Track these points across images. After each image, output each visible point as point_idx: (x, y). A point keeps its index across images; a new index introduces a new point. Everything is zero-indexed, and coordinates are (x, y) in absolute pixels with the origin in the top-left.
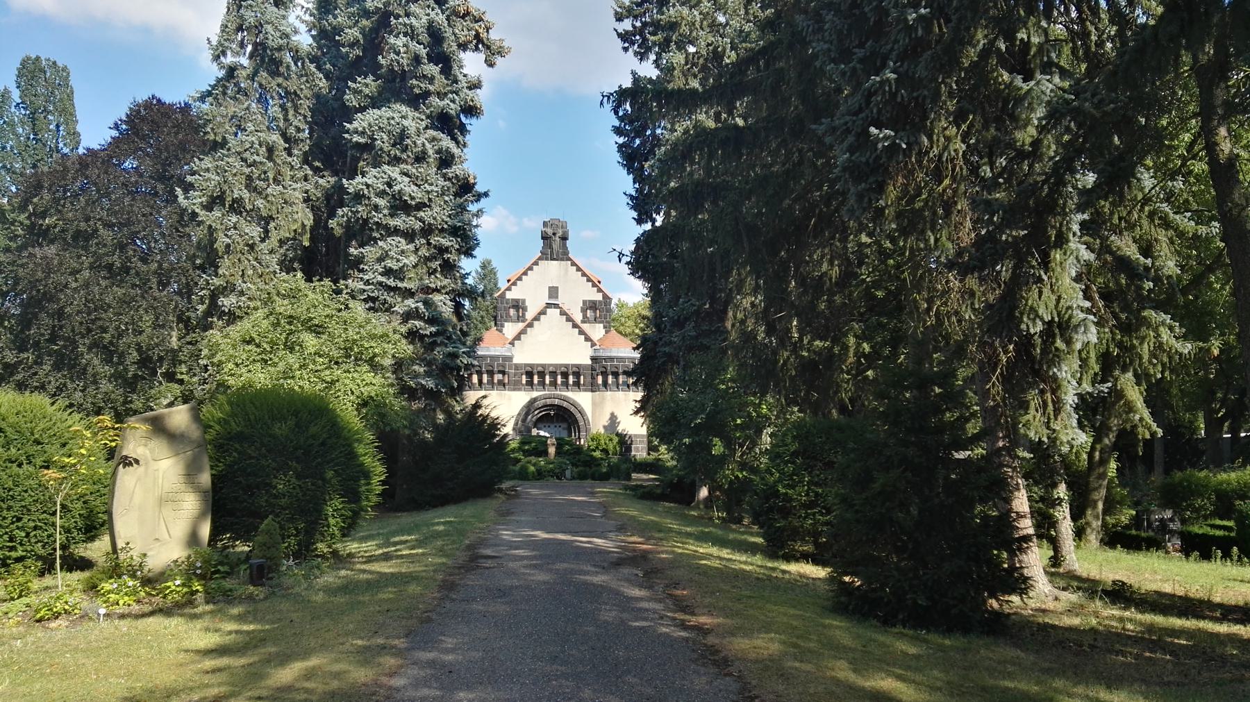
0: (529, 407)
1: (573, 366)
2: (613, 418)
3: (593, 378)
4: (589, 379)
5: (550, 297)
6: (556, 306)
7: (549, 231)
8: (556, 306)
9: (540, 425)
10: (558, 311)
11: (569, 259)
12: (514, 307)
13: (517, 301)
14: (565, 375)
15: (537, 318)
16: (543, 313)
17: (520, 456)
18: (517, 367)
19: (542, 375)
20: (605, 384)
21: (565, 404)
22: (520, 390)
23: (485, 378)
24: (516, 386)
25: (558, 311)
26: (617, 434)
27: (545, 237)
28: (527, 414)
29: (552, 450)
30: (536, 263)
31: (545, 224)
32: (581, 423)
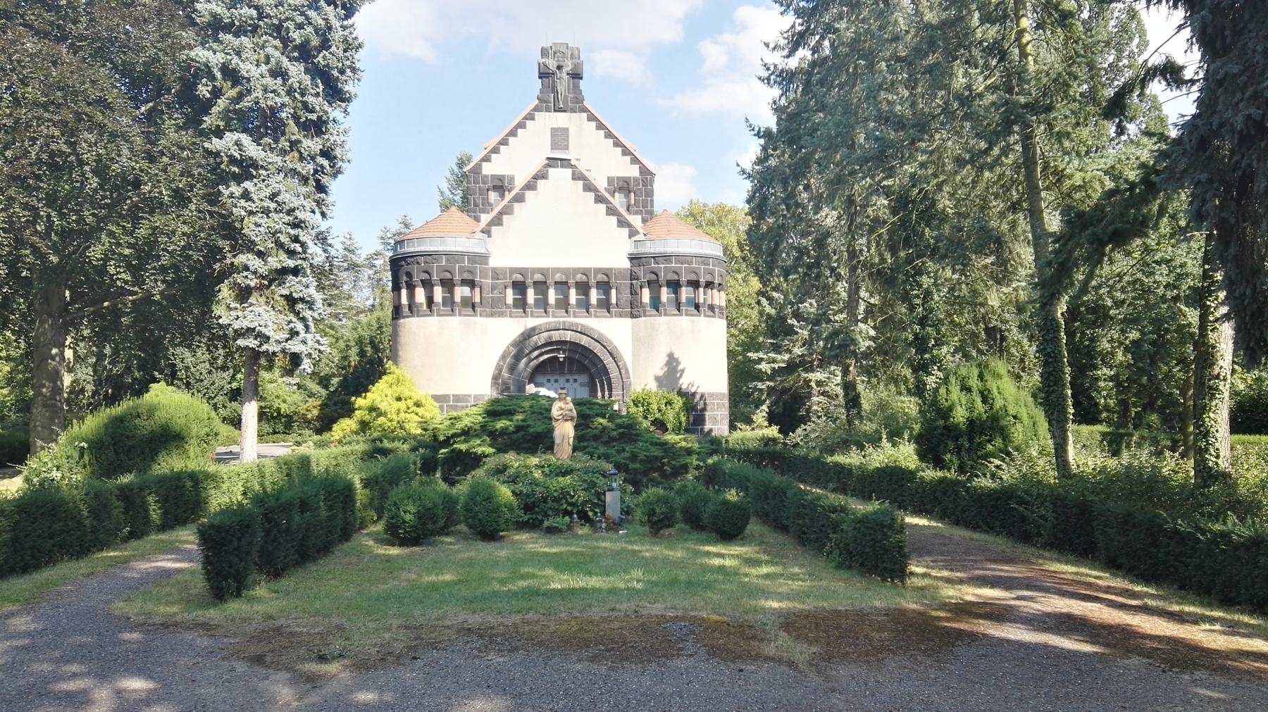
0: (521, 345)
1: (597, 271)
2: (672, 362)
3: (633, 292)
4: (626, 295)
5: (554, 146)
6: (565, 163)
7: (552, 64)
8: (565, 163)
9: (540, 379)
10: (568, 172)
11: (584, 110)
12: (495, 188)
13: (500, 178)
14: (583, 288)
15: (530, 186)
16: (541, 175)
17: (481, 447)
18: (496, 273)
19: (541, 287)
20: (656, 303)
21: (584, 341)
22: (502, 314)
23: (438, 293)
24: (495, 308)
25: (568, 172)
26: (681, 393)
27: (544, 75)
28: (518, 358)
29: (565, 431)
30: (530, 117)
31: (544, 52)
32: (614, 373)
